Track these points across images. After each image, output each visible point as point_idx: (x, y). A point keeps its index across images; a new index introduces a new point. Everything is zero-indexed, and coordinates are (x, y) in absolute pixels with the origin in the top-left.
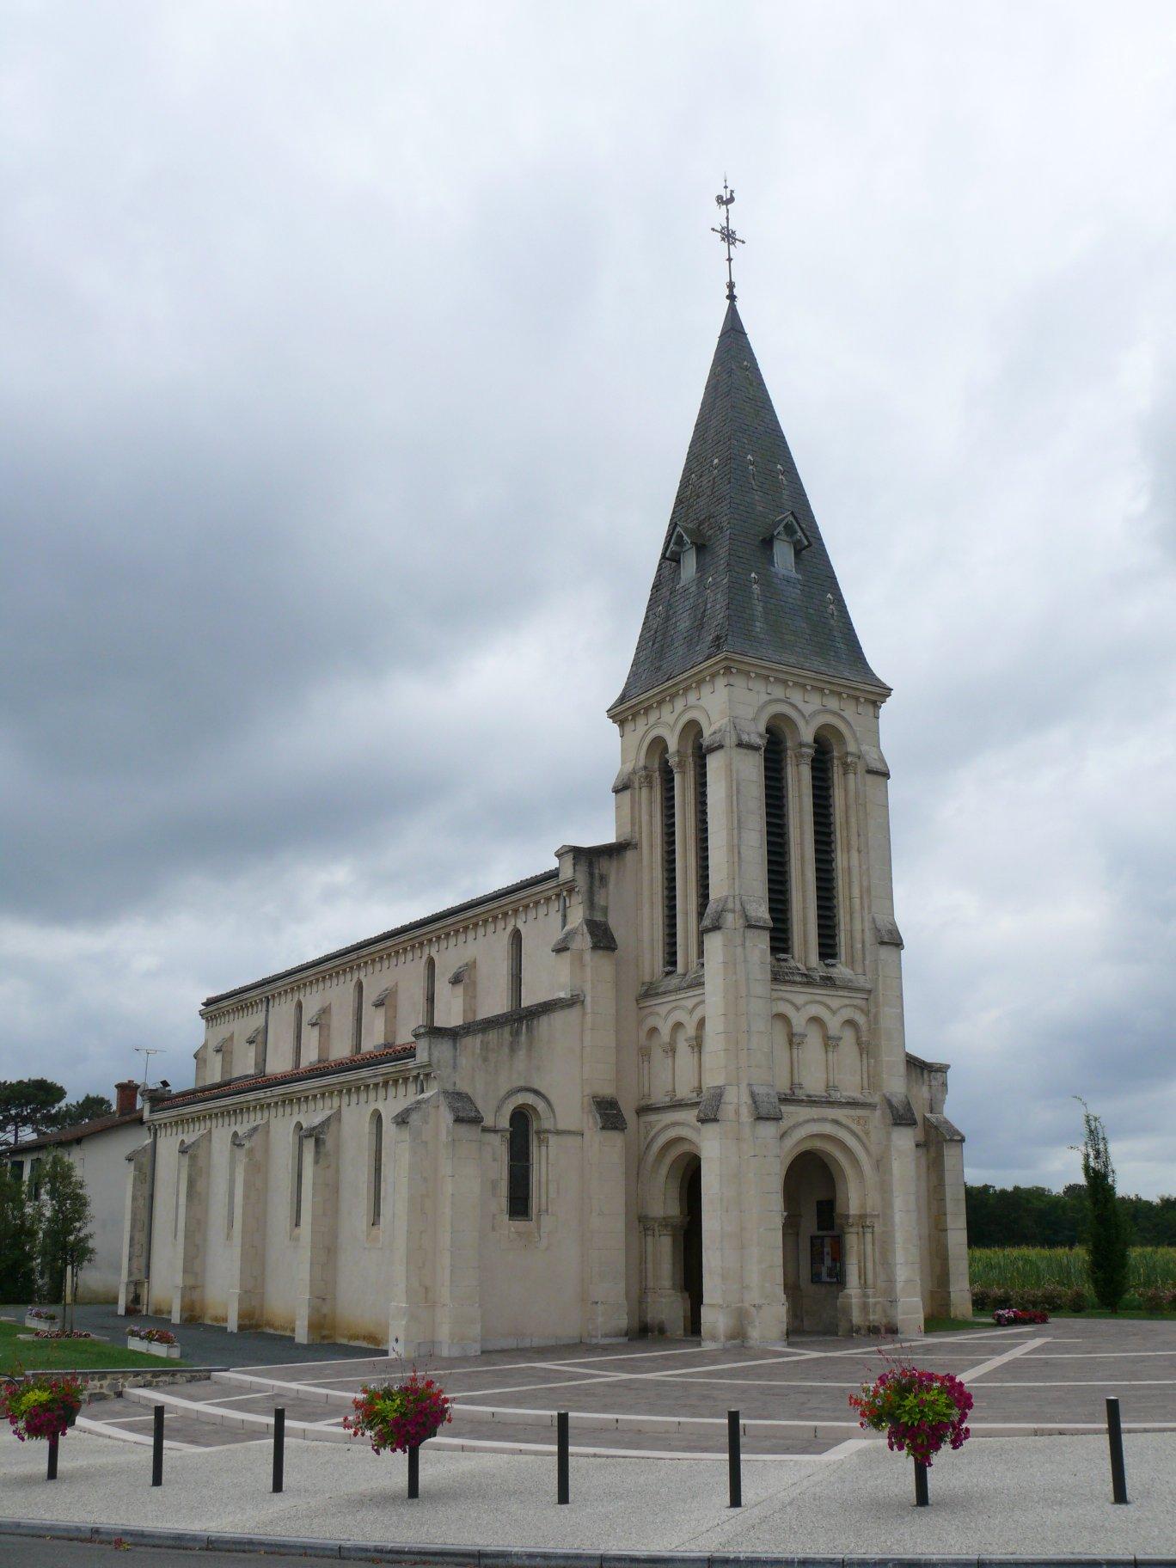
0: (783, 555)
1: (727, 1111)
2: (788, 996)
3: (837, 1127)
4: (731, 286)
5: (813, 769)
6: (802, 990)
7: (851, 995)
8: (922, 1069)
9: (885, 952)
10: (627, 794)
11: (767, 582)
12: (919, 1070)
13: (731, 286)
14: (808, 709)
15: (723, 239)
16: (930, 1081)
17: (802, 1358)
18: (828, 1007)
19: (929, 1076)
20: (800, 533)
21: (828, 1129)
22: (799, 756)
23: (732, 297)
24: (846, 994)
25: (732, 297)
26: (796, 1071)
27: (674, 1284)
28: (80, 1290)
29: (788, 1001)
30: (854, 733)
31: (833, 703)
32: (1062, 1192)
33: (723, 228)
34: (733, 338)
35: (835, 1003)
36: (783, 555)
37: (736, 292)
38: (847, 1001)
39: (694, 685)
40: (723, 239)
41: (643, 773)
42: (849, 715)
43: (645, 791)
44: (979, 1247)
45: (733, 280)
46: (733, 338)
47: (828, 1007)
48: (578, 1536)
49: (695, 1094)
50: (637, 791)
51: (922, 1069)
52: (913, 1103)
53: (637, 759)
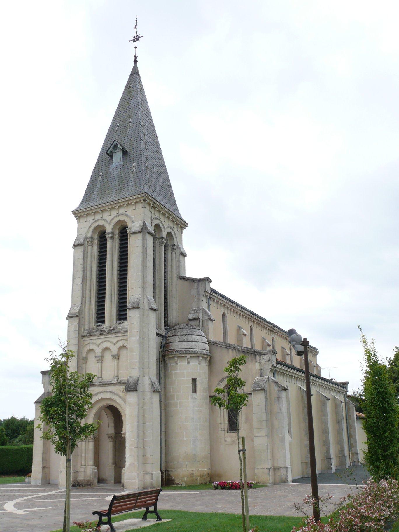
1: (140, 387)
2: (91, 341)
3: (112, 394)
4: (136, 57)
6: (100, 337)
7: (122, 335)
8: (255, 355)
10: (81, 249)
12: (253, 355)
13: (136, 57)
15: (139, 40)
16: (260, 360)
17: (54, 492)
18: (111, 342)
19: (260, 357)
21: (108, 395)
23: (136, 61)
24: (120, 335)
25: (136, 61)
26: (116, 367)
29: (91, 343)
33: (138, 36)
34: (135, 73)
35: (115, 340)
37: (137, 59)
38: (121, 338)
39: (93, 214)
41: (90, 240)
43: (90, 247)
44: (312, 479)
46: (135, 73)
47: (111, 342)
49: (115, 380)
50: (86, 246)
51: (255, 355)
52: (140, 381)
53: (88, 232)
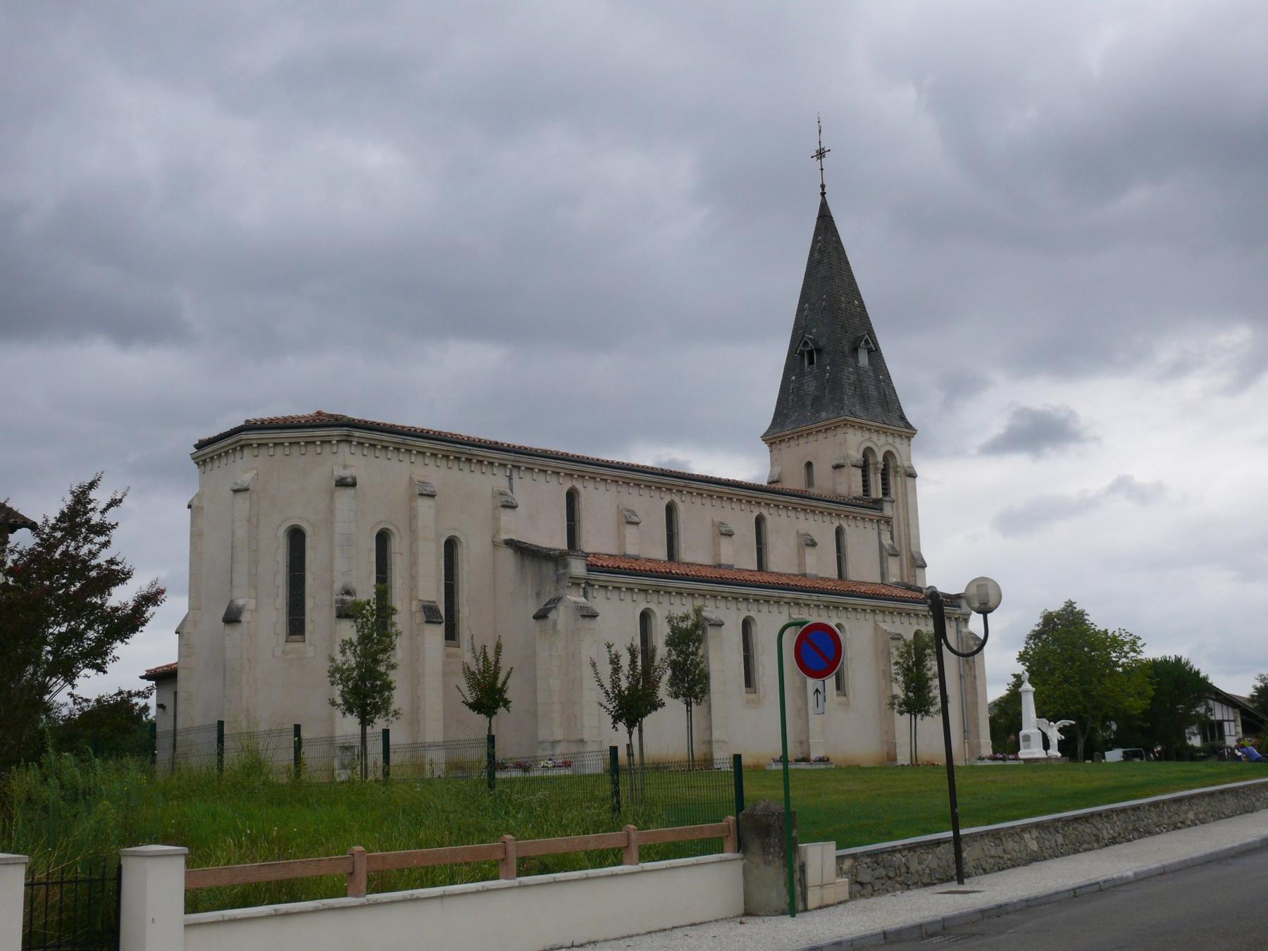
0: (863, 359)
4: (823, 186)
5: (882, 474)
9: (909, 480)
11: (857, 367)
13: (823, 186)
14: (879, 443)
20: (871, 344)
22: (876, 469)
23: (823, 194)
25: (823, 194)
27: (1015, 903)
28: (645, 758)
30: (900, 454)
31: (890, 439)
32: (991, 753)
34: (825, 221)
36: (863, 359)
40: (817, 151)
42: (898, 446)
45: (824, 183)
46: (825, 221)
48: (58, 612)
